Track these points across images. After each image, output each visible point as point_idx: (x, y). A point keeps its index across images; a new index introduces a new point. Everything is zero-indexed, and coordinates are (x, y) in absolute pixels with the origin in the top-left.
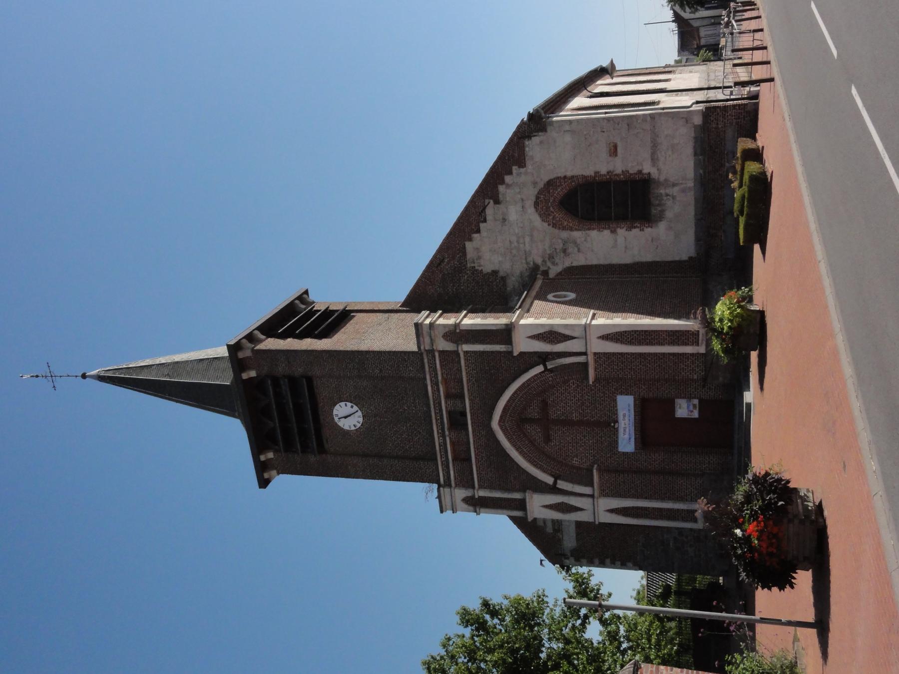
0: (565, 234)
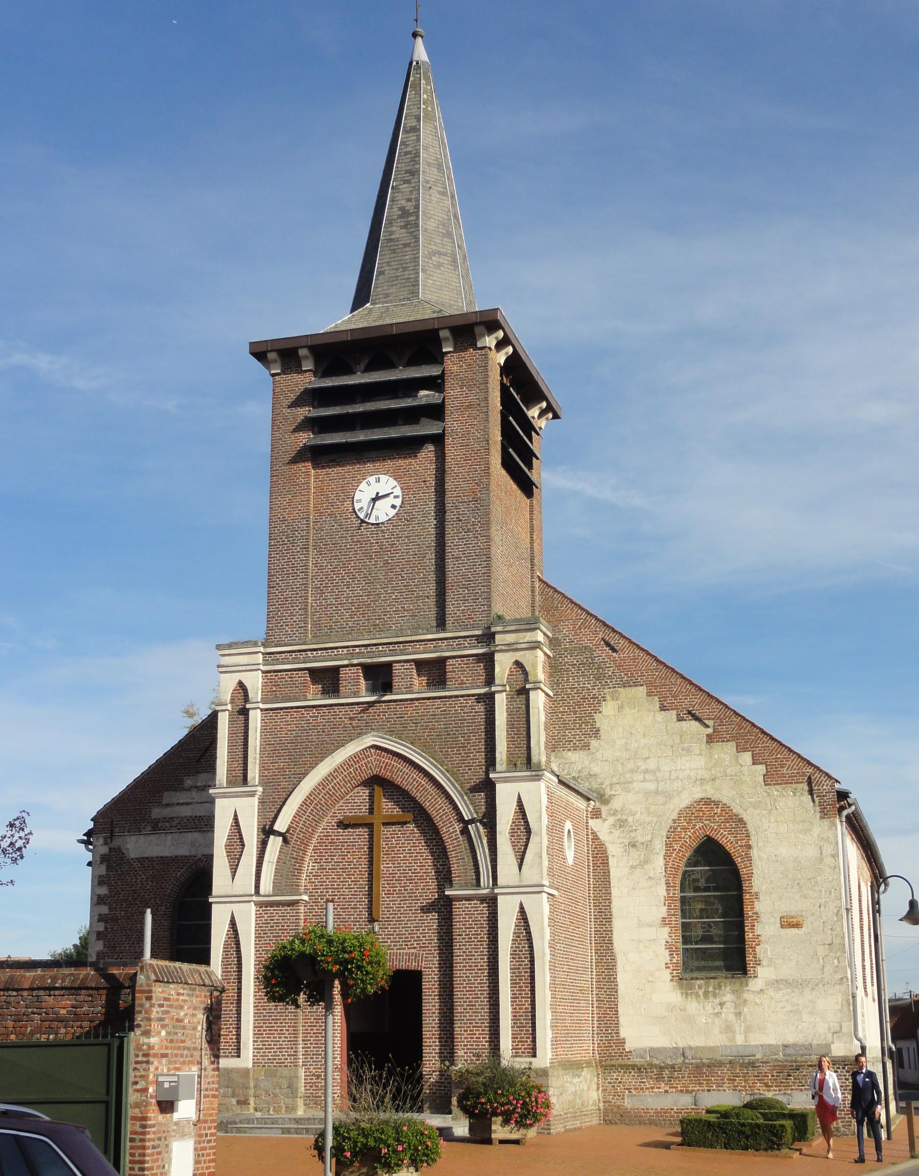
0: (659, 846)
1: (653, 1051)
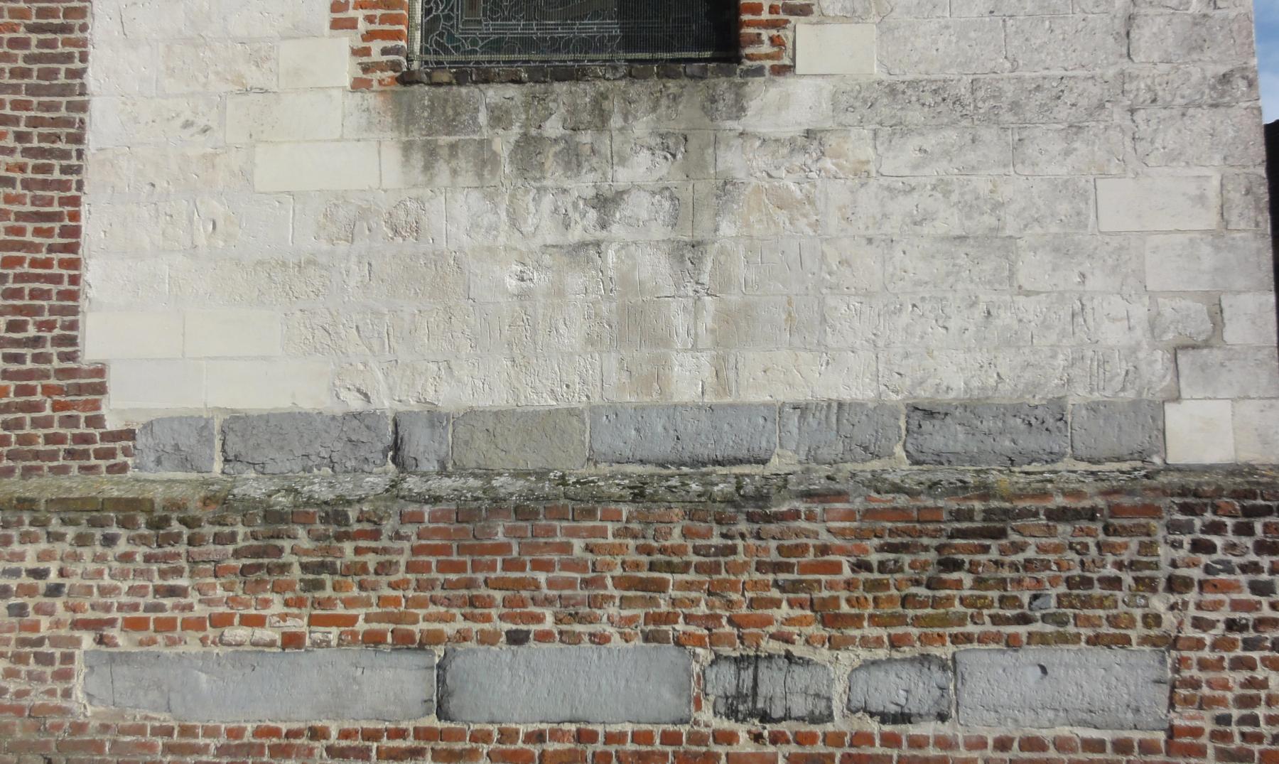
1: (242, 433)
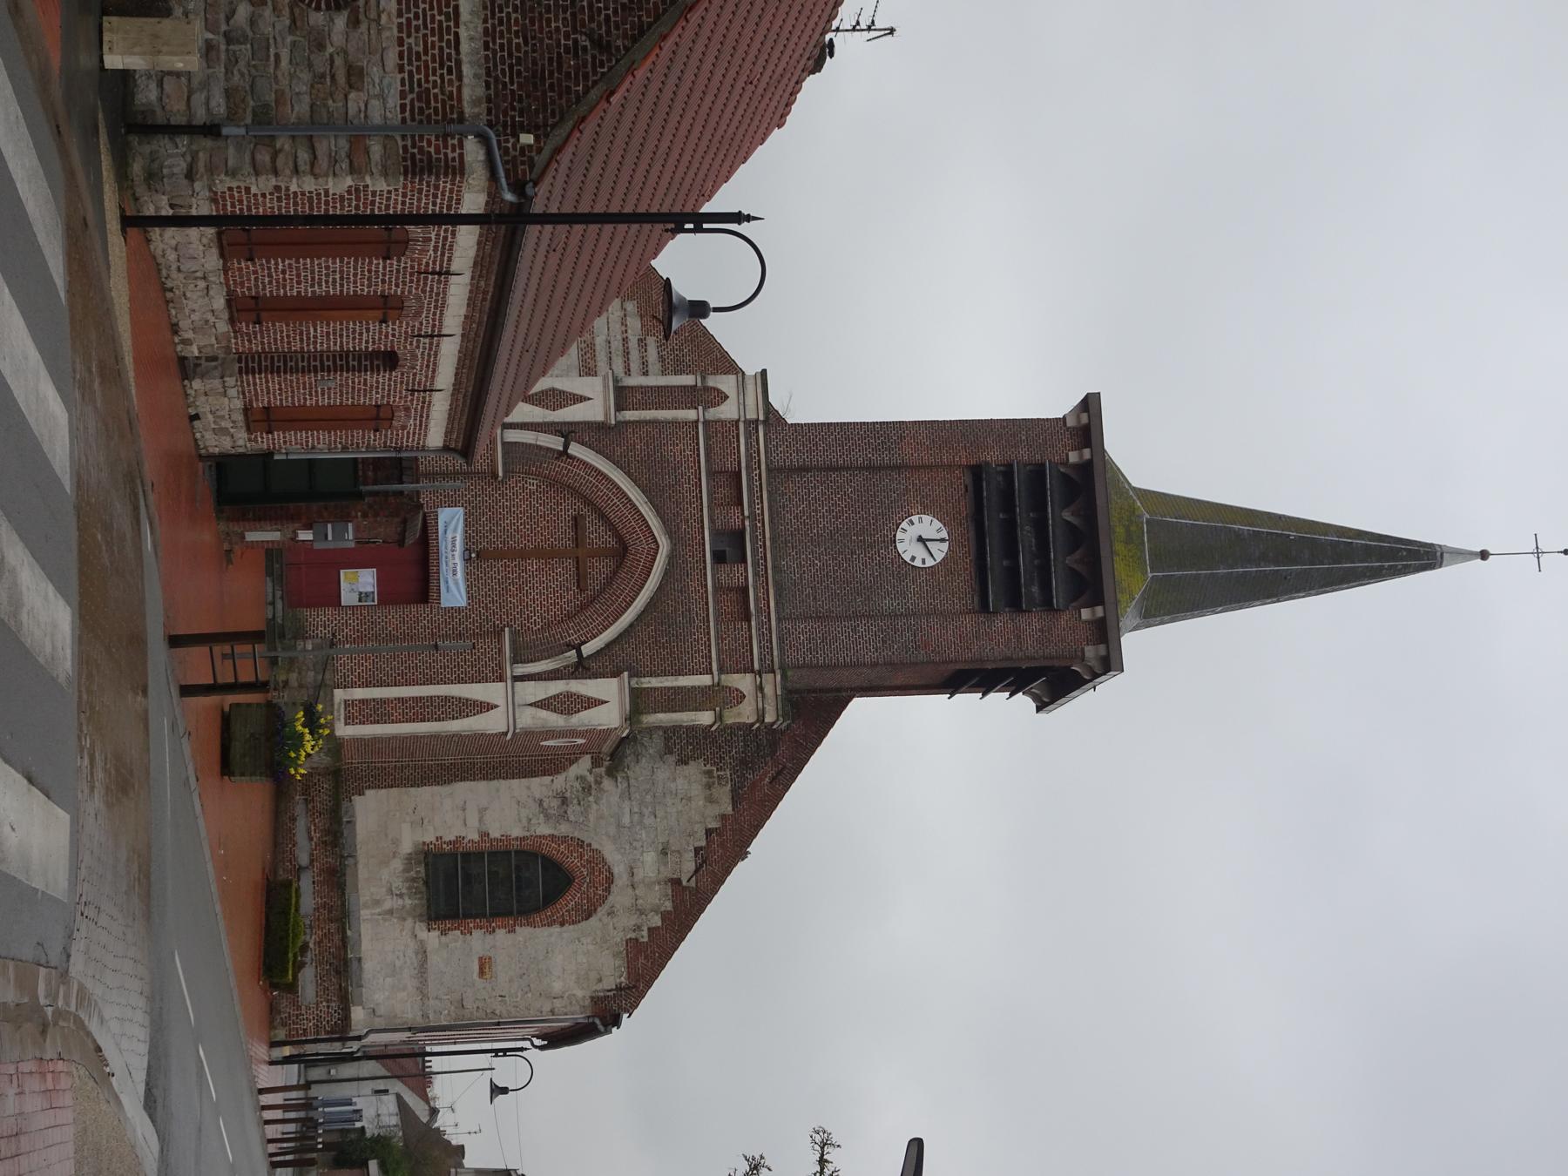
0: (564, 829)
